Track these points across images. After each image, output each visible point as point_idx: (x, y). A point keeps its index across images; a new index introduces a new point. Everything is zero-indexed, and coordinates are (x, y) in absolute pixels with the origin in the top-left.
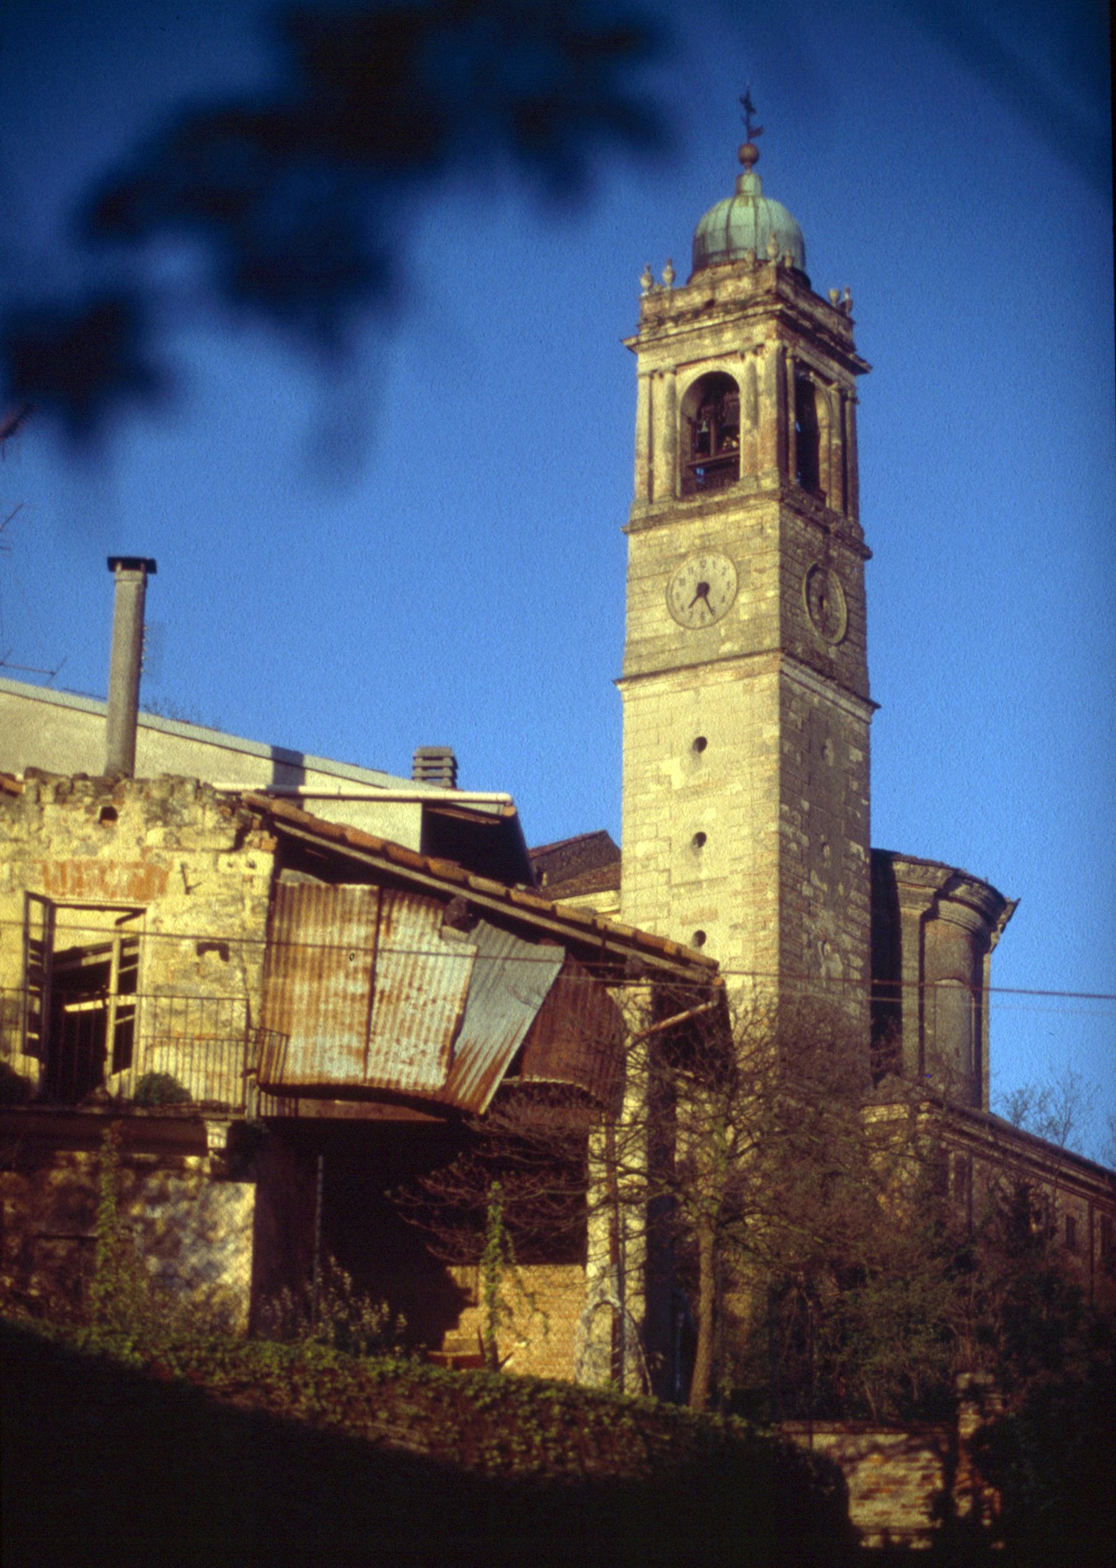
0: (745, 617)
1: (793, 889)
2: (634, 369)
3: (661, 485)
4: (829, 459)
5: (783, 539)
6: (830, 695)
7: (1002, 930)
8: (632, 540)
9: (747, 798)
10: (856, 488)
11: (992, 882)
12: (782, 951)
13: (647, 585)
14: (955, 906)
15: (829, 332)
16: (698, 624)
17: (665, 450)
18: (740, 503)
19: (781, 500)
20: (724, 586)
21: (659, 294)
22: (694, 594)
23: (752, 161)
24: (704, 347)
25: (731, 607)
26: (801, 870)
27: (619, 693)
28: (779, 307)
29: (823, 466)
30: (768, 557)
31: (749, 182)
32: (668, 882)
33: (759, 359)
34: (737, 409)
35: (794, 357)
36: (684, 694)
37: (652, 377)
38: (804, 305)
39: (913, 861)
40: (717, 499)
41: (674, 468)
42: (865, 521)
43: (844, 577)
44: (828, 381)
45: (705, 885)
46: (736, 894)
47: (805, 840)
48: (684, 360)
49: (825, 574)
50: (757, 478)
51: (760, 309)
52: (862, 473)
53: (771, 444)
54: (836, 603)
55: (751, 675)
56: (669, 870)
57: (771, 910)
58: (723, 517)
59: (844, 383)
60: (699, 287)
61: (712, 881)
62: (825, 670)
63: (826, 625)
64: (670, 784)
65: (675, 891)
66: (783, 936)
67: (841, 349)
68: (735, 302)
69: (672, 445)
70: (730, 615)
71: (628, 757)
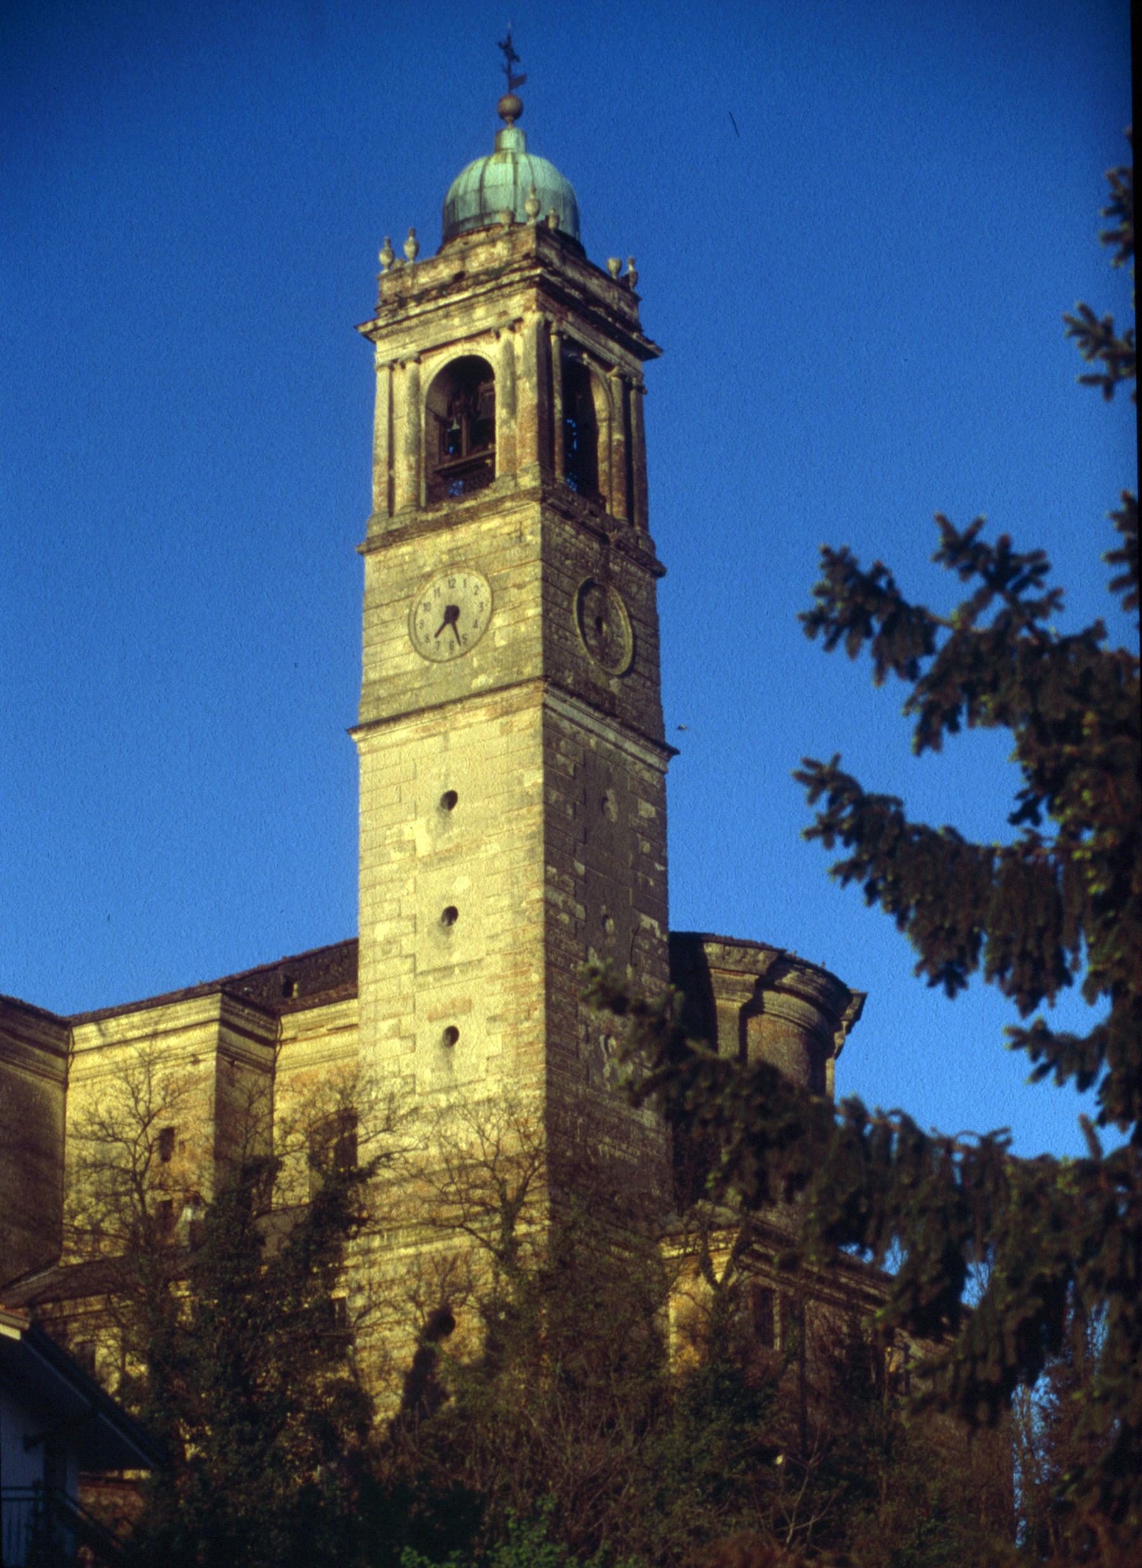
0: (501, 642)
1: (565, 969)
2: (372, 360)
3: (402, 495)
4: (609, 458)
5: (546, 547)
6: (611, 736)
7: (849, 1030)
8: (370, 561)
9: (502, 863)
10: (644, 492)
11: (829, 968)
12: (550, 1046)
13: (386, 613)
14: (784, 997)
15: (608, 308)
16: (447, 655)
17: (408, 453)
18: (494, 507)
19: (543, 500)
20: (476, 608)
21: (401, 270)
22: (441, 621)
23: (516, 115)
24: (453, 327)
25: (486, 630)
26: (575, 946)
27: (354, 745)
28: (538, 271)
29: (603, 467)
30: (529, 569)
31: (510, 138)
32: (414, 969)
33: (517, 336)
34: (492, 398)
35: (559, 334)
36: (431, 741)
37: (392, 369)
38: (571, 273)
39: (728, 942)
40: (467, 504)
41: (418, 474)
42: (655, 529)
43: (629, 598)
44: (607, 366)
45: (457, 971)
46: (493, 978)
47: (580, 910)
48: (428, 344)
49: (604, 591)
50: (515, 477)
51: (516, 277)
52: (652, 475)
53: (530, 435)
54: (619, 626)
55: (508, 711)
56: (413, 956)
57: (536, 996)
58: (474, 526)
59: (627, 369)
60: (446, 259)
61: (466, 966)
62: (604, 705)
63: (605, 652)
64: (415, 849)
65: (420, 979)
66: (552, 1027)
67: (623, 329)
68: (487, 272)
69: (415, 446)
70: (483, 644)
71: (364, 821)
